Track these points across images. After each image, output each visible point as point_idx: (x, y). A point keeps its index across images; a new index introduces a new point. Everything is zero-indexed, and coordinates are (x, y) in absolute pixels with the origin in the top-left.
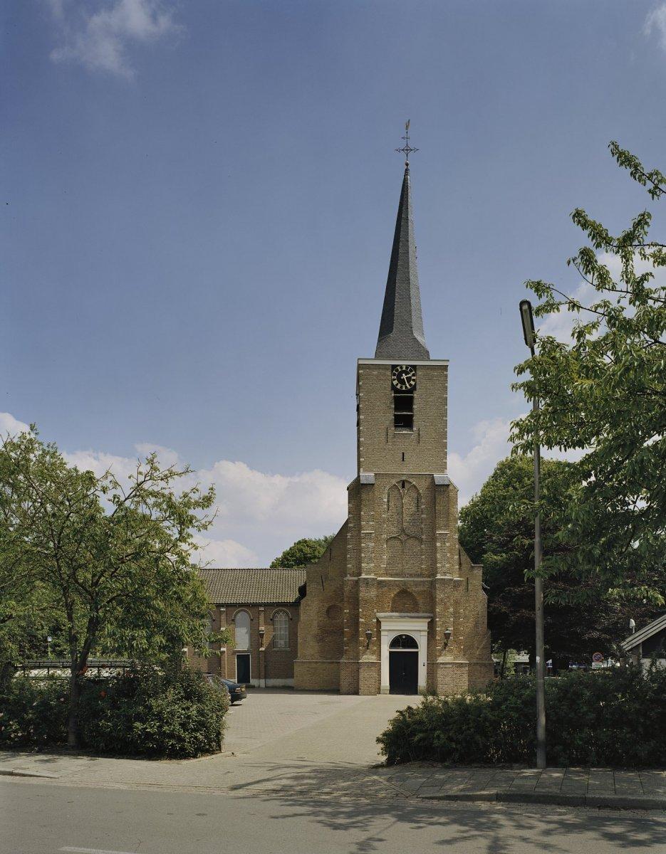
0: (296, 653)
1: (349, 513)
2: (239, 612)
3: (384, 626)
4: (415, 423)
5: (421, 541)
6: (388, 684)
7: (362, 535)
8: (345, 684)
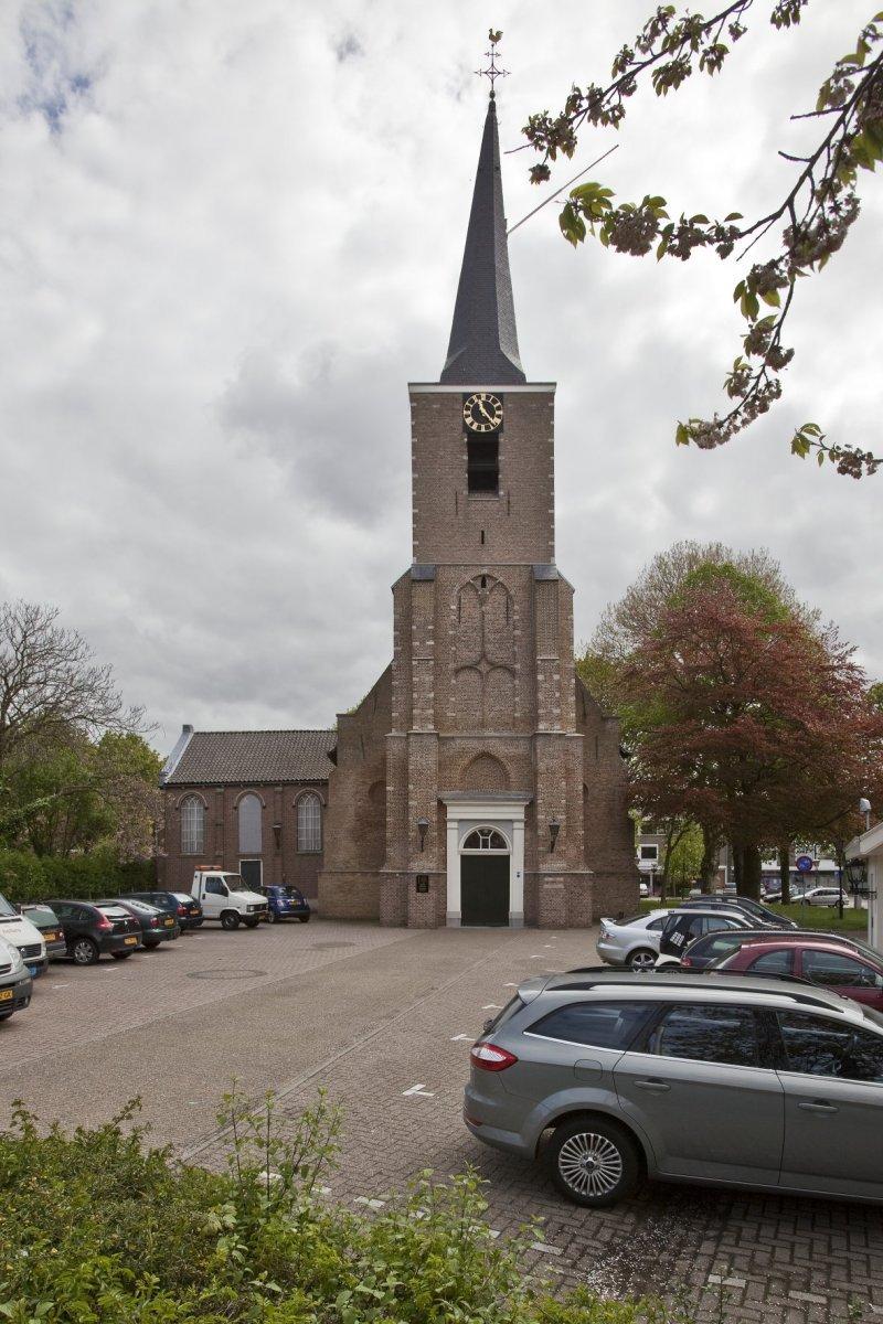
0: (785, 364)
1: (396, 645)
2: (243, 796)
3: (454, 813)
4: (501, 484)
5: (513, 673)
6: (459, 910)
7: (414, 663)
8: (387, 911)
